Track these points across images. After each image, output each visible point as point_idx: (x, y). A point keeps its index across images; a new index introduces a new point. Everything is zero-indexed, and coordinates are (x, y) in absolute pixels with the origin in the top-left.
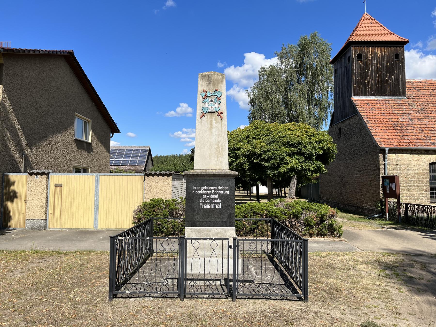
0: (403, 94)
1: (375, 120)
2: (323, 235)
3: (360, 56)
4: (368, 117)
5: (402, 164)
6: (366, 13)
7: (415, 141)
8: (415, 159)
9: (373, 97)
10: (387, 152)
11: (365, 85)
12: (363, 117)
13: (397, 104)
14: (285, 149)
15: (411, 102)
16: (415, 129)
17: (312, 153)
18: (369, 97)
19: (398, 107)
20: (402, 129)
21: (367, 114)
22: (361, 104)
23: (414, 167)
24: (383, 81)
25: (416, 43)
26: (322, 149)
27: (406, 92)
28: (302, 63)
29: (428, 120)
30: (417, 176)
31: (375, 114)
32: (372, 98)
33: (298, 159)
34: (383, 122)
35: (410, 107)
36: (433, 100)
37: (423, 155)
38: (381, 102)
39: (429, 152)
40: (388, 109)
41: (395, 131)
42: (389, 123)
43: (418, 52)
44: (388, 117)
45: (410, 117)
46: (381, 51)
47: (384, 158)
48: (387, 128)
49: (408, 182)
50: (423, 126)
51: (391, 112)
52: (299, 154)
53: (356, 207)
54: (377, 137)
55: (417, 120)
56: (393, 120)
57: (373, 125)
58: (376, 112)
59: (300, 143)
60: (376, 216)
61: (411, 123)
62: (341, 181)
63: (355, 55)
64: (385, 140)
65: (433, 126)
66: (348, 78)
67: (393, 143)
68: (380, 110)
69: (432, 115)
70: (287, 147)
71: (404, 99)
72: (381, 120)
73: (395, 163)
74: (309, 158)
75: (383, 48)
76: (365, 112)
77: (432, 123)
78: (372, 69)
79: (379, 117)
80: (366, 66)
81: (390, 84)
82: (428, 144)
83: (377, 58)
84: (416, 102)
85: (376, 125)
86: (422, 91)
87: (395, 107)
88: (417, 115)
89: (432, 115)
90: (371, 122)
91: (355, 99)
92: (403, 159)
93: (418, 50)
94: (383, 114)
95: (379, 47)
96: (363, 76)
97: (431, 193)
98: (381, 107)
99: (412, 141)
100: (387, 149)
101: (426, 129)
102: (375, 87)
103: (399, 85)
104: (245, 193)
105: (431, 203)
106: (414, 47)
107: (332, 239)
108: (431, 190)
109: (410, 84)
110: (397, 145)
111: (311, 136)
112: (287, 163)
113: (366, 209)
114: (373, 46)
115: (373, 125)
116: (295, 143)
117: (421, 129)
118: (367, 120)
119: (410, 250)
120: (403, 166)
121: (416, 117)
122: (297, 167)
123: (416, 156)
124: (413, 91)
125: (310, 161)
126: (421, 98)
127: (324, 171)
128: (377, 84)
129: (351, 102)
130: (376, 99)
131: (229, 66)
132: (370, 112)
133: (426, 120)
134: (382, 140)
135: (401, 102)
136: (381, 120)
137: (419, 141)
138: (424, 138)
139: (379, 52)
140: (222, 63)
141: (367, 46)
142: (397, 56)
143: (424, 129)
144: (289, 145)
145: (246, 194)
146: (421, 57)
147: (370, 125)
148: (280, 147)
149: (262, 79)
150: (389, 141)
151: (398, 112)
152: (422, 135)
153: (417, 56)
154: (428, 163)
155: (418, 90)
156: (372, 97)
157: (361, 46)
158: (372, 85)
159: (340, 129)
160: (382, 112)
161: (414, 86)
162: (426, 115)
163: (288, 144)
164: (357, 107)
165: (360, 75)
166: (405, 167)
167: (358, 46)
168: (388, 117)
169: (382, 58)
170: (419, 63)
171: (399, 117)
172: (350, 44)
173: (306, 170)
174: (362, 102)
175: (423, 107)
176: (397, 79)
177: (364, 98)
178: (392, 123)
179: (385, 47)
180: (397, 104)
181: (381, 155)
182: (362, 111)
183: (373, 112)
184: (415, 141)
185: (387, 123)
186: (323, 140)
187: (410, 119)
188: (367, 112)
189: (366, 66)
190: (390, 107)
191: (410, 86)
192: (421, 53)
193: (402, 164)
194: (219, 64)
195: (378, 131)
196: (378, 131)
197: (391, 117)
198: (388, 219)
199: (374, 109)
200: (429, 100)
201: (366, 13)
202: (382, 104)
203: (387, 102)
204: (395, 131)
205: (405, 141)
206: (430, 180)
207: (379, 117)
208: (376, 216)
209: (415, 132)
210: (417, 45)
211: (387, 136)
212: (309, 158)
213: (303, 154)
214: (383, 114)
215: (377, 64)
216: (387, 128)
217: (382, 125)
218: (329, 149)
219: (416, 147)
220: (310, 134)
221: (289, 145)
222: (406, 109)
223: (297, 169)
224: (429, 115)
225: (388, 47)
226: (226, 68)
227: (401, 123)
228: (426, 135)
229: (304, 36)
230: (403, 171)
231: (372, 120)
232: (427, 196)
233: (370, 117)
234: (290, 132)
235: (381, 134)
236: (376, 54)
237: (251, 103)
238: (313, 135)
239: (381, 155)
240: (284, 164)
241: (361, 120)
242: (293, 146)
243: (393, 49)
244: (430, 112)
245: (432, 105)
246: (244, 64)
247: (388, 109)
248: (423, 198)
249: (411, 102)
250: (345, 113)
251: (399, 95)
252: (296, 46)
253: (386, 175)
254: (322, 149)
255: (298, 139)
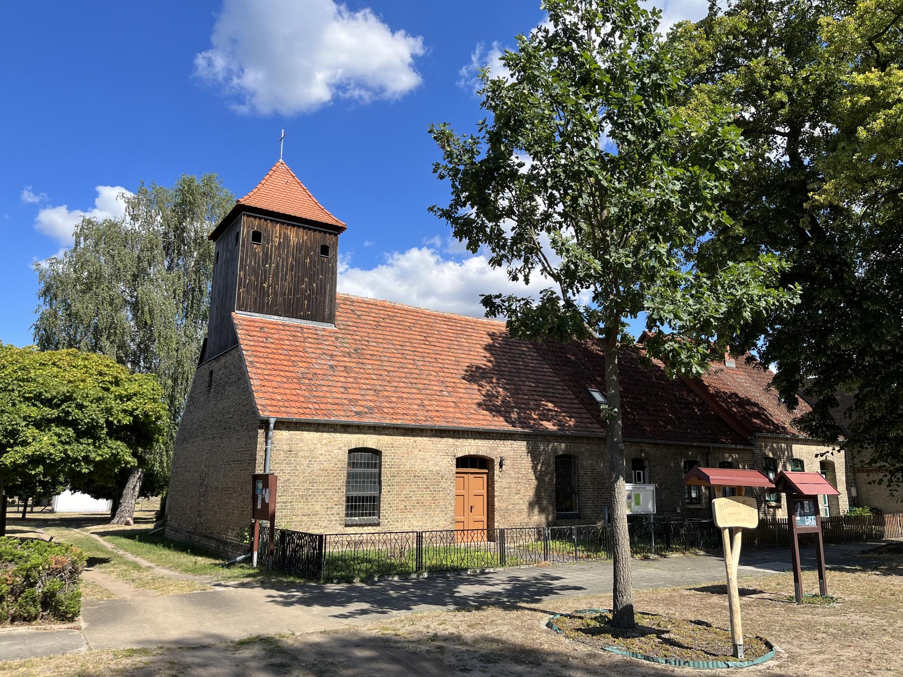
0: (331, 319)
1: (267, 361)
2: (28, 619)
3: (257, 236)
4: (255, 353)
5: (300, 451)
6: (281, 160)
7: (329, 407)
8: (325, 441)
9: (276, 317)
10: (272, 426)
11: (263, 293)
12: (245, 353)
13: (315, 336)
14: (26, 409)
15: (340, 336)
16: (335, 384)
17: (97, 423)
18: (267, 316)
19: (316, 341)
20: (312, 382)
21: (254, 349)
22: (248, 328)
23: (321, 458)
24: (297, 290)
25: (432, 237)
26: (131, 414)
27: (334, 315)
28: (180, 230)
29: (362, 371)
30: (325, 473)
31: (269, 350)
32: (274, 319)
33: (59, 435)
34: (280, 367)
35: (338, 344)
36: (379, 336)
37: (339, 435)
38: (287, 328)
39: (349, 430)
40: (297, 343)
41: (297, 386)
42: (291, 369)
43: (433, 254)
44: (293, 359)
45: (331, 363)
46: (297, 235)
47: (267, 437)
48: (284, 380)
49: (306, 485)
50: (351, 380)
51: (300, 349)
52: (61, 421)
53: (218, 540)
54: (261, 395)
55: (343, 369)
56: (300, 364)
57: (259, 371)
58: (273, 346)
59: (68, 398)
60: (239, 558)
61: (331, 373)
62: (201, 485)
63: (248, 232)
64: (275, 403)
65: (367, 382)
66: (233, 273)
67: (288, 410)
68: (282, 342)
69: (371, 362)
70: (35, 405)
71: (330, 327)
72: (279, 362)
73: (286, 447)
74: (89, 432)
75: (301, 229)
76: (252, 343)
77: (367, 376)
78: (277, 265)
79: (276, 356)
80: (266, 257)
81: (308, 298)
82: (349, 414)
83: (288, 245)
84: (349, 337)
85: (266, 372)
86: (365, 318)
87: (311, 340)
88: (345, 359)
89: (371, 362)
90: (258, 365)
91: (239, 316)
92: (302, 440)
93: (433, 250)
94: (286, 352)
95: (294, 226)
96: (259, 273)
97: (347, 507)
98: (286, 338)
99: (323, 406)
100: (272, 421)
101: (354, 385)
102: (280, 299)
103: (324, 301)
104: (18, 512)
105: (346, 526)
106: (427, 243)
107: (48, 627)
108: (348, 501)
109: (348, 303)
110: (294, 415)
111: (111, 383)
112: (25, 443)
113: (231, 543)
114: (283, 223)
115: (259, 371)
116: (55, 397)
117: (345, 385)
118: (251, 359)
119: (197, 635)
120: (301, 454)
121: (342, 364)
122: (51, 454)
123: (325, 435)
124: (349, 315)
125: (90, 441)
126: (360, 329)
127: (128, 463)
128: (285, 295)
129: (230, 319)
130: (279, 322)
131: (55, 204)
132: (262, 344)
133: (357, 370)
134: (269, 402)
135: (323, 333)
136: (279, 362)
137: (335, 407)
138: (346, 402)
139: (294, 236)
140: (36, 194)
141: (271, 221)
142: (325, 250)
143: (349, 385)
144: (37, 399)
145: (20, 515)
146: (437, 263)
147: (254, 370)
148: (14, 405)
149: (82, 246)
150: (281, 404)
151: (313, 350)
152: (344, 396)
153: (432, 260)
154: (346, 449)
155: (359, 316)
156: (272, 317)
157: (260, 219)
158: (276, 294)
159: (211, 372)
160: (285, 347)
161: (353, 308)
162: (361, 361)
163: (38, 397)
164: (239, 331)
165: (255, 272)
166: (305, 457)
167: (255, 217)
168: (293, 359)
169: (299, 247)
170: (434, 272)
171: (314, 361)
172: (240, 209)
173: (76, 460)
174: (252, 324)
175: (359, 346)
176: (321, 291)
177: (257, 316)
178: (296, 369)
179: (304, 228)
180: (315, 336)
181: (261, 432)
182: (246, 342)
183: (268, 345)
184: (329, 407)
185: (287, 368)
186: (135, 395)
187: (331, 367)
188: (257, 344)
189: (266, 257)
190: (302, 339)
191: (347, 307)
192: (438, 257)
193: (300, 451)
194: (26, 193)
195: (266, 383)
196: (266, 383)
197: (299, 359)
198: (255, 564)
199: (271, 340)
200: (371, 335)
201: (281, 160)
202: (288, 333)
203: (299, 329)
204: (297, 386)
205: (311, 406)
206: (348, 482)
207: (276, 356)
208: (239, 558)
209: (334, 390)
210: (433, 241)
211: (281, 394)
212: (89, 432)
213: (74, 424)
214: (286, 352)
215: (287, 256)
216: (284, 380)
217: (277, 373)
218: (146, 415)
219: (326, 418)
220: (107, 378)
221: (37, 399)
222: (329, 348)
223: (49, 458)
224: (365, 361)
225: (310, 229)
226: (44, 208)
227: (314, 371)
228: (351, 397)
229: (187, 177)
230: (300, 465)
231: (262, 360)
232: (338, 514)
233: (259, 354)
234: (55, 369)
235: (271, 390)
236: (287, 238)
237: (45, 293)
238: (117, 382)
239: (261, 432)
240: (17, 445)
241: (241, 359)
242: (48, 403)
243: (318, 235)
244: (368, 357)
245: (375, 344)
246: (94, 207)
247: (297, 343)
248: (333, 518)
249: (340, 336)
250: (222, 344)
251: (323, 320)
252: (170, 190)
253: (267, 472)
254: (131, 414)
255: (64, 389)
